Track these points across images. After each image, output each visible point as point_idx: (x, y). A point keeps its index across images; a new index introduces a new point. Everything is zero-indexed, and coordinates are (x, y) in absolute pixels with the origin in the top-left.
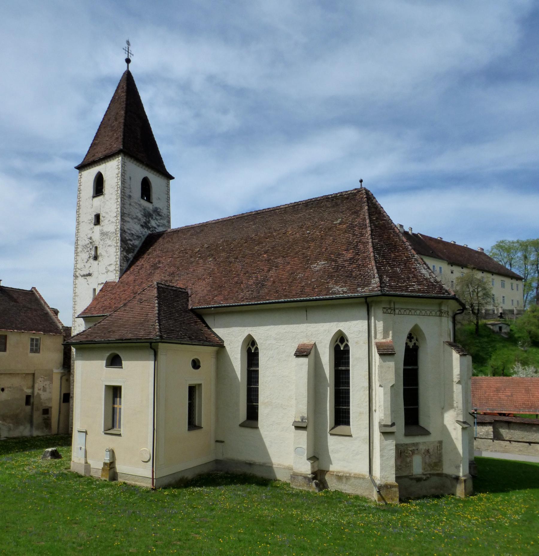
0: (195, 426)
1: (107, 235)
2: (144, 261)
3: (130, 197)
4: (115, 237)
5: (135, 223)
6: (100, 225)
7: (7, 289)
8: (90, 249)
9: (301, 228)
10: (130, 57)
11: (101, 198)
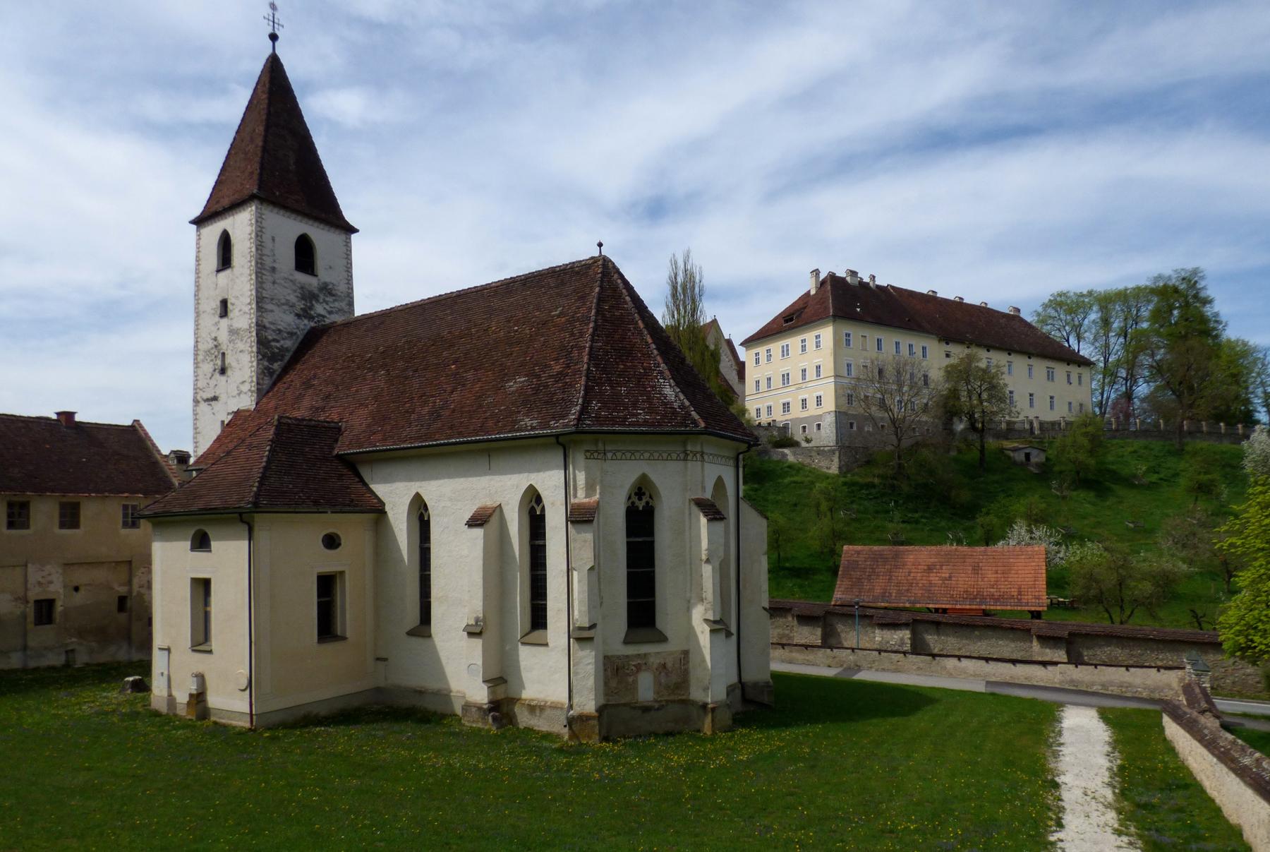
0: (337, 636)
1: (238, 334)
2: (295, 375)
3: (273, 269)
4: (249, 338)
5: (284, 312)
6: (228, 318)
7: (88, 425)
8: (215, 357)
9: (509, 321)
10: (277, 32)
11: (228, 272)
